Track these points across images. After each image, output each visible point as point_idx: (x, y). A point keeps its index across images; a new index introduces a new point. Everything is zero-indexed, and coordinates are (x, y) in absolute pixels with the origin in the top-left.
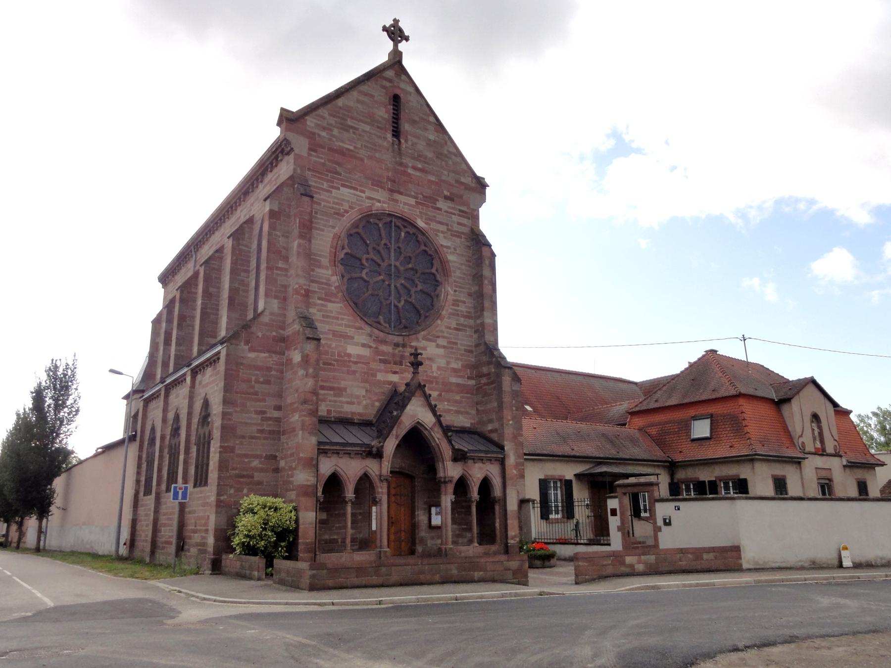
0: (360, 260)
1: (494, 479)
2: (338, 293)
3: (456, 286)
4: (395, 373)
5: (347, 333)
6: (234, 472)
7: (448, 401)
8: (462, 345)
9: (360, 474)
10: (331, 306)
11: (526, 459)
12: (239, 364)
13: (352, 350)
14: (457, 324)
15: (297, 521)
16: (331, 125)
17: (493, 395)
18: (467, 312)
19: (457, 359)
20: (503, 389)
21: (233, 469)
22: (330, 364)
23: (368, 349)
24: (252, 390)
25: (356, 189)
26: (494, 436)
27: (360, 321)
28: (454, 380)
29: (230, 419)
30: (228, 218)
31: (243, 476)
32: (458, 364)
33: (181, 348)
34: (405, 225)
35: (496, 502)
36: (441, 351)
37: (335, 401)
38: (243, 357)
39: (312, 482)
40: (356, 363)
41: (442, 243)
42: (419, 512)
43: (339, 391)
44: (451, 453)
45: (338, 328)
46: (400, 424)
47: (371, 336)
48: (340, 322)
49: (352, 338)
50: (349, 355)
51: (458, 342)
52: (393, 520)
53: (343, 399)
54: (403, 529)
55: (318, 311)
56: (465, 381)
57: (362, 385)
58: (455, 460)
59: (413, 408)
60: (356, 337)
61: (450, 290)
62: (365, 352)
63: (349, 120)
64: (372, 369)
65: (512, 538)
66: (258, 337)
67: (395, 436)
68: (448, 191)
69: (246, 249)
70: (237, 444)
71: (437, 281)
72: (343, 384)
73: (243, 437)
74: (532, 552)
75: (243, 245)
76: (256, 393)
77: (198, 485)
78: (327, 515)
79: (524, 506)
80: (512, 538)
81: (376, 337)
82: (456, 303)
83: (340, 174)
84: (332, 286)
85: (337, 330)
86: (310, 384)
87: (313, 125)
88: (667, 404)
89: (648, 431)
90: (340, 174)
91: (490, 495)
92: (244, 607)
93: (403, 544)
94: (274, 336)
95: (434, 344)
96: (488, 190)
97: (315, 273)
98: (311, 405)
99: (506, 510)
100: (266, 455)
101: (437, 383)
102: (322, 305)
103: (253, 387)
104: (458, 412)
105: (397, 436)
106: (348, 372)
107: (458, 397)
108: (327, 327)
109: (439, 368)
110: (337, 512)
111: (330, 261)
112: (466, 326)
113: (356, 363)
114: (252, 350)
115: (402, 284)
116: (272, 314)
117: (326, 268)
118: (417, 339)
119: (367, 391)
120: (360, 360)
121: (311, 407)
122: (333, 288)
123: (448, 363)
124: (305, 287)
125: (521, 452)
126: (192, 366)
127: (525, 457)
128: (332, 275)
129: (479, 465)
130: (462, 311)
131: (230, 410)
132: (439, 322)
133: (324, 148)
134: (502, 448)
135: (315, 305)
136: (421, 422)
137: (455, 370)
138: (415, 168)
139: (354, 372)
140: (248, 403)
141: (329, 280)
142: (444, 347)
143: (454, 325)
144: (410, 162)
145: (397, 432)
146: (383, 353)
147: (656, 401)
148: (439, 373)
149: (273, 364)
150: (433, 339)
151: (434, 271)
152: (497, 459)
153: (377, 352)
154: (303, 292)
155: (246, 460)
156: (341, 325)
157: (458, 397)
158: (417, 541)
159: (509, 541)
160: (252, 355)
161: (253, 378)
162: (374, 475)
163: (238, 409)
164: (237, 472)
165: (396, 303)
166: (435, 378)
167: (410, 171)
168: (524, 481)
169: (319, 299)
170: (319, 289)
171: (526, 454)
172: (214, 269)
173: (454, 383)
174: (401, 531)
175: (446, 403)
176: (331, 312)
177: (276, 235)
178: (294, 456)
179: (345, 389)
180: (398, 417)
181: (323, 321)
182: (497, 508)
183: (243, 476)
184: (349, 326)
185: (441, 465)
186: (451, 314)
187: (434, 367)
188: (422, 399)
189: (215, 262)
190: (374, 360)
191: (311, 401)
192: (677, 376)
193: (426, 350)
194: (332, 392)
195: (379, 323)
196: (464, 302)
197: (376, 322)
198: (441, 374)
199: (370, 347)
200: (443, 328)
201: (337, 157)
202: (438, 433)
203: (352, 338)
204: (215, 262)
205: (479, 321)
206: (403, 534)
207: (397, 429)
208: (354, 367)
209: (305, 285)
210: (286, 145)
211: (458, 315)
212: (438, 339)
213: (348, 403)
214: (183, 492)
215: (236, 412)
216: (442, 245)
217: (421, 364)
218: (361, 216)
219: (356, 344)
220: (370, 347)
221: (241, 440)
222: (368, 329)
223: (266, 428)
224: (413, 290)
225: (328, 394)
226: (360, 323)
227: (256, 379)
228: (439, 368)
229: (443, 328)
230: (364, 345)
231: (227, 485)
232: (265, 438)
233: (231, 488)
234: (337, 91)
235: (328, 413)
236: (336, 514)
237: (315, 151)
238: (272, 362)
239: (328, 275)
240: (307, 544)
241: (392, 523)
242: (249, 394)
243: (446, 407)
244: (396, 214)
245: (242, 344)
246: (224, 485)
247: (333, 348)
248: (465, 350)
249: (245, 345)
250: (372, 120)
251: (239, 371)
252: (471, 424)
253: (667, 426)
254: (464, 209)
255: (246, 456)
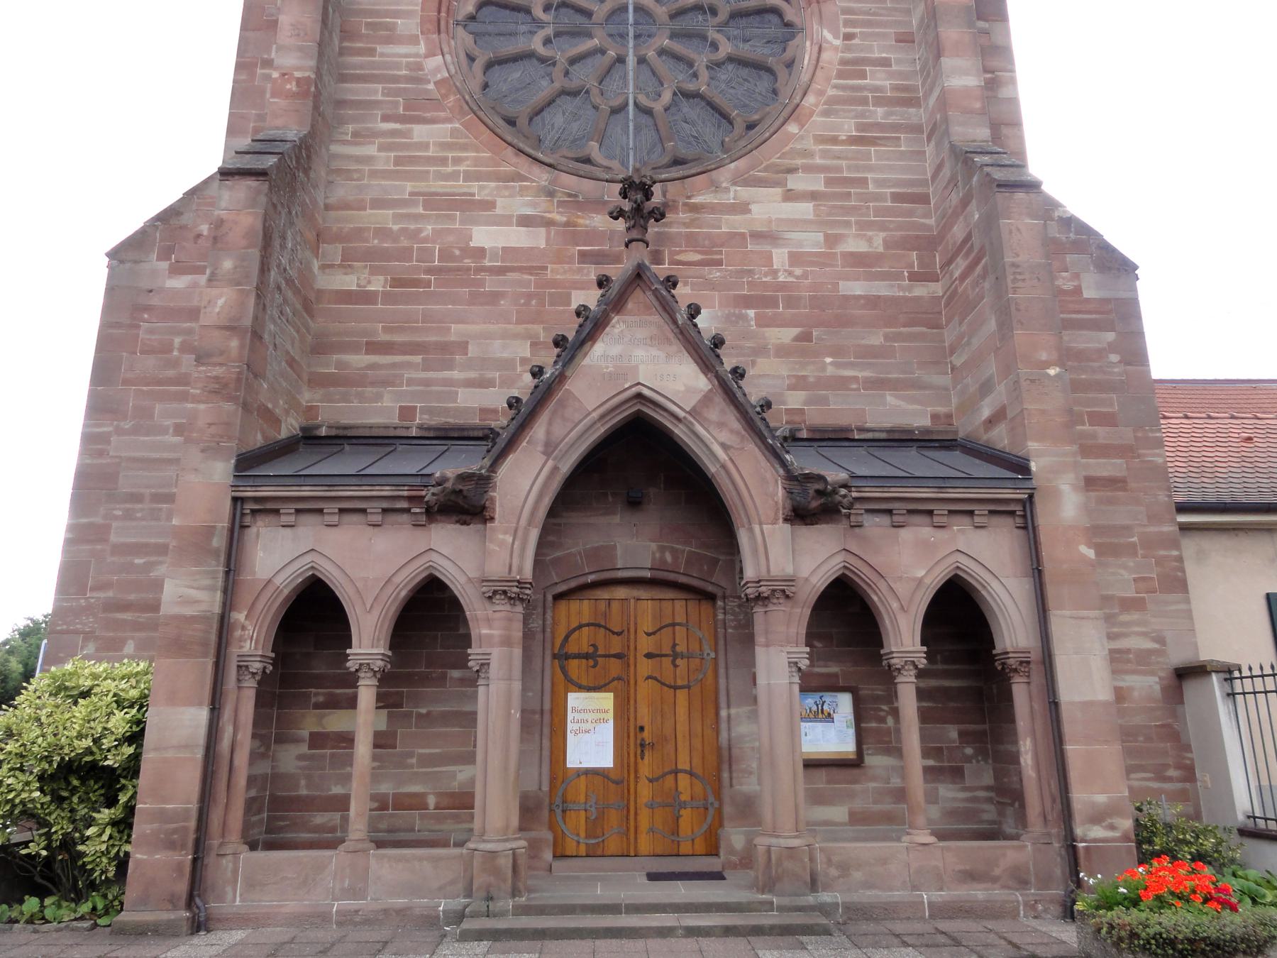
0: (528, 11)
1: (995, 584)
2: (445, 96)
3: (847, 23)
5: (473, 195)
6: (102, 595)
7: (837, 352)
8: (878, 183)
9: (406, 580)
10: (420, 132)
11: (1185, 528)
13: (484, 236)
14: (861, 127)
15: (136, 737)
18: (896, 88)
19: (864, 226)
20: (1008, 259)
22: (416, 283)
23: (543, 230)
24: (171, 373)
26: (1000, 438)
27: (514, 160)
28: (857, 288)
31: (126, 607)
32: (870, 240)
36: (805, 209)
37: (427, 383)
39: (204, 607)
40: (501, 271)
42: (733, 711)
43: (445, 352)
44: (780, 493)
45: (438, 186)
46: (562, 404)
47: (551, 194)
48: (450, 169)
49: (490, 205)
50: (481, 252)
51: (869, 176)
52: (646, 734)
53: (456, 374)
54: (683, 764)
55: (380, 149)
56: (900, 288)
57: (520, 328)
58: (800, 515)
59: (615, 350)
60: (500, 202)
61: (827, 35)
62: (535, 239)
64: (554, 284)
65: (1097, 817)
66: (199, 236)
67: (540, 448)
70: (116, 518)
71: (788, 25)
72: (456, 331)
73: (136, 498)
74: (1119, 915)
78: (390, 716)
79: (1192, 688)
80: (1097, 817)
81: (570, 195)
82: (853, 67)
84: (429, 82)
85: (440, 190)
86: (221, 302)
91: (992, 645)
93: (686, 813)
95: (778, 191)
97: (377, 58)
98: (221, 365)
99: (1054, 705)
101: (791, 302)
102: (393, 133)
103: (176, 363)
104: (879, 384)
106: (474, 299)
107: (876, 339)
108: (409, 186)
109: (795, 259)
110: (424, 711)
111: (423, 21)
112: (895, 127)
113: (501, 271)
114: (177, 270)
115: (662, 52)
117: (413, 40)
118: (715, 187)
119: (534, 345)
120: (513, 260)
121: (218, 371)
122: (431, 86)
123: (831, 240)
124: (298, 74)
125: (1162, 497)
127: (1183, 518)
128: (430, 54)
129: (919, 532)
130: (876, 89)
131: (105, 429)
132: (792, 128)
134: (1020, 467)
135: (376, 134)
136: (646, 392)
137: (857, 260)
139: (495, 297)
140: (158, 407)
141: (419, 67)
142: (813, 196)
143: (848, 127)
145: (548, 433)
146: (592, 235)
148: (798, 271)
150: (777, 176)
152: (999, 510)
153: (571, 233)
154: (292, 86)
155: (138, 561)
156: (454, 176)
157: (876, 339)
158: (728, 809)
159: (1079, 831)
160: (180, 283)
161: (177, 341)
162: (463, 580)
163: (127, 425)
164: (110, 594)
165: (643, 100)
166: (783, 286)
168: (1188, 601)
169: (386, 118)
170: (388, 95)
171: (1182, 508)
173: (859, 297)
174: (676, 772)
175: (828, 360)
176: (425, 146)
179: (463, 347)
181: (397, 171)
182: (1020, 692)
183: (126, 607)
184: (478, 177)
186: (832, 101)
187: (780, 257)
188: (656, 318)
190: (560, 258)
191: (222, 353)
194: (418, 359)
195: (587, 160)
196: (885, 63)
197: (578, 160)
198: (805, 276)
199: (549, 223)
202: (721, 425)
203: (490, 205)
206: (684, 780)
207: (550, 423)
208: (490, 284)
209: (298, 69)
211: (864, 101)
212: (789, 176)
213: (470, 383)
215: (119, 431)
217: (658, 215)
219: (505, 221)
220: (549, 223)
221: (128, 506)
222: (542, 177)
224: (702, 59)
225: (409, 365)
226: (514, 163)
227: (183, 343)
228: (795, 259)
229: (809, 144)
230: (525, 221)
231: (76, 632)
233: (86, 640)
235: (401, 417)
236: (420, 716)
239: (417, 55)
240: (162, 816)
241: (642, 745)
242: (160, 382)
243: (830, 371)
246: (67, 632)
247: (425, 240)
248: (897, 197)
249: (159, 259)
251: (138, 327)
252: (935, 417)
255: (140, 549)
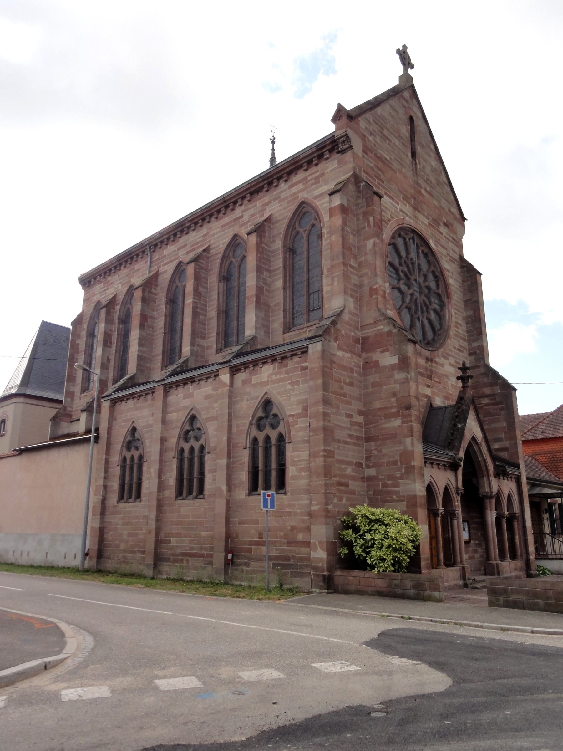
4: (428, 386)
12: (332, 362)
16: (375, 131)
17: (500, 415)
21: (335, 476)
24: (342, 391)
25: (393, 200)
29: (329, 421)
30: (216, 218)
33: (144, 349)
34: (423, 244)
35: (516, 518)
38: (333, 355)
41: (445, 266)
63: (385, 130)
68: (445, 218)
69: (268, 248)
75: (264, 243)
76: (344, 395)
77: (185, 494)
83: (383, 182)
87: (364, 127)
88: (555, 436)
89: (538, 458)
90: (383, 182)
92: (483, 631)
94: (353, 336)
96: (466, 223)
100: (356, 462)
103: (342, 388)
105: (464, 449)
114: (340, 348)
116: (350, 313)
126: (231, 364)
133: (372, 152)
138: (425, 190)
144: (423, 185)
147: (542, 432)
149: (354, 365)
151: (440, 291)
155: (343, 467)
160: (340, 353)
167: (423, 192)
172: (202, 268)
177: (347, 231)
178: (397, 465)
180: (463, 429)
185: (486, 480)
189: (203, 262)
192: (552, 413)
193: (444, 367)
200: (451, 348)
201: (380, 165)
204: (203, 262)
205: (475, 344)
210: (343, 142)
214: (270, 499)
216: (445, 268)
218: (397, 227)
223: (355, 434)
231: (332, 493)
232: (354, 444)
234: (376, 98)
237: (366, 154)
238: (353, 364)
244: (418, 232)
245: (333, 340)
250: (400, 137)
253: (559, 454)
254: (455, 237)
